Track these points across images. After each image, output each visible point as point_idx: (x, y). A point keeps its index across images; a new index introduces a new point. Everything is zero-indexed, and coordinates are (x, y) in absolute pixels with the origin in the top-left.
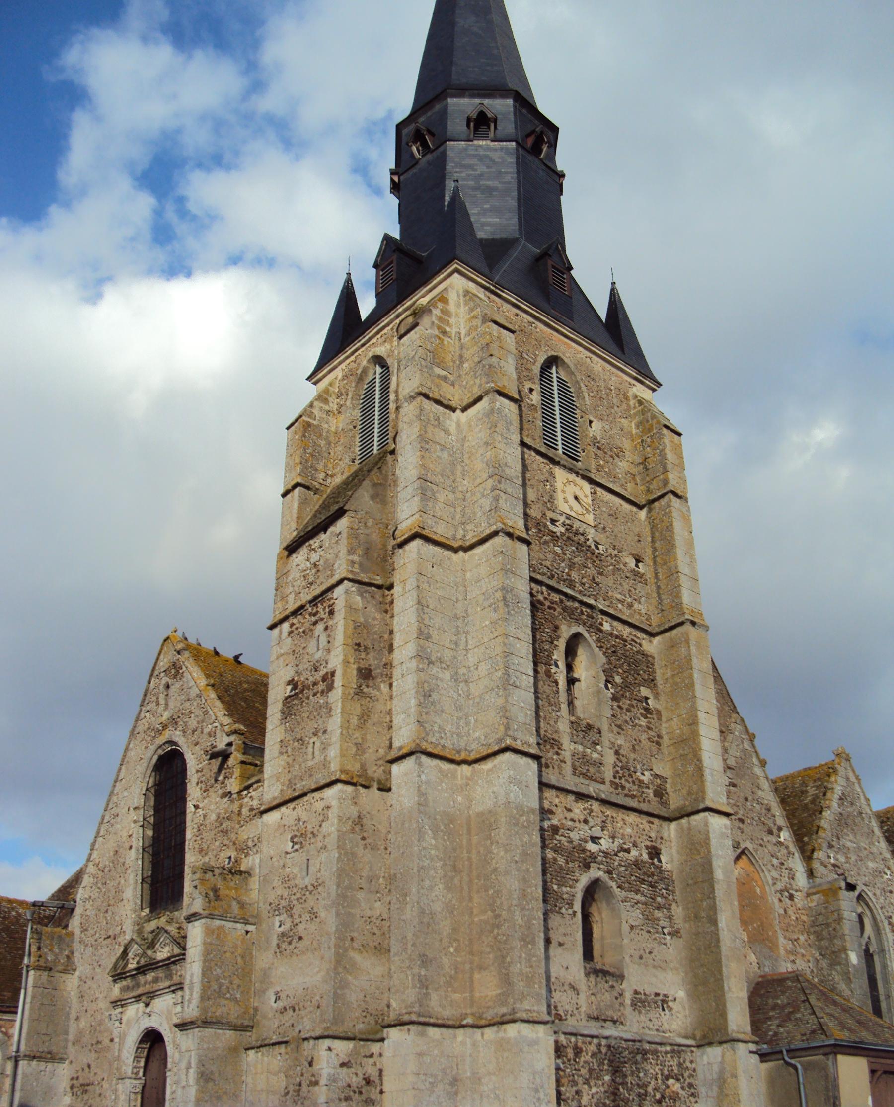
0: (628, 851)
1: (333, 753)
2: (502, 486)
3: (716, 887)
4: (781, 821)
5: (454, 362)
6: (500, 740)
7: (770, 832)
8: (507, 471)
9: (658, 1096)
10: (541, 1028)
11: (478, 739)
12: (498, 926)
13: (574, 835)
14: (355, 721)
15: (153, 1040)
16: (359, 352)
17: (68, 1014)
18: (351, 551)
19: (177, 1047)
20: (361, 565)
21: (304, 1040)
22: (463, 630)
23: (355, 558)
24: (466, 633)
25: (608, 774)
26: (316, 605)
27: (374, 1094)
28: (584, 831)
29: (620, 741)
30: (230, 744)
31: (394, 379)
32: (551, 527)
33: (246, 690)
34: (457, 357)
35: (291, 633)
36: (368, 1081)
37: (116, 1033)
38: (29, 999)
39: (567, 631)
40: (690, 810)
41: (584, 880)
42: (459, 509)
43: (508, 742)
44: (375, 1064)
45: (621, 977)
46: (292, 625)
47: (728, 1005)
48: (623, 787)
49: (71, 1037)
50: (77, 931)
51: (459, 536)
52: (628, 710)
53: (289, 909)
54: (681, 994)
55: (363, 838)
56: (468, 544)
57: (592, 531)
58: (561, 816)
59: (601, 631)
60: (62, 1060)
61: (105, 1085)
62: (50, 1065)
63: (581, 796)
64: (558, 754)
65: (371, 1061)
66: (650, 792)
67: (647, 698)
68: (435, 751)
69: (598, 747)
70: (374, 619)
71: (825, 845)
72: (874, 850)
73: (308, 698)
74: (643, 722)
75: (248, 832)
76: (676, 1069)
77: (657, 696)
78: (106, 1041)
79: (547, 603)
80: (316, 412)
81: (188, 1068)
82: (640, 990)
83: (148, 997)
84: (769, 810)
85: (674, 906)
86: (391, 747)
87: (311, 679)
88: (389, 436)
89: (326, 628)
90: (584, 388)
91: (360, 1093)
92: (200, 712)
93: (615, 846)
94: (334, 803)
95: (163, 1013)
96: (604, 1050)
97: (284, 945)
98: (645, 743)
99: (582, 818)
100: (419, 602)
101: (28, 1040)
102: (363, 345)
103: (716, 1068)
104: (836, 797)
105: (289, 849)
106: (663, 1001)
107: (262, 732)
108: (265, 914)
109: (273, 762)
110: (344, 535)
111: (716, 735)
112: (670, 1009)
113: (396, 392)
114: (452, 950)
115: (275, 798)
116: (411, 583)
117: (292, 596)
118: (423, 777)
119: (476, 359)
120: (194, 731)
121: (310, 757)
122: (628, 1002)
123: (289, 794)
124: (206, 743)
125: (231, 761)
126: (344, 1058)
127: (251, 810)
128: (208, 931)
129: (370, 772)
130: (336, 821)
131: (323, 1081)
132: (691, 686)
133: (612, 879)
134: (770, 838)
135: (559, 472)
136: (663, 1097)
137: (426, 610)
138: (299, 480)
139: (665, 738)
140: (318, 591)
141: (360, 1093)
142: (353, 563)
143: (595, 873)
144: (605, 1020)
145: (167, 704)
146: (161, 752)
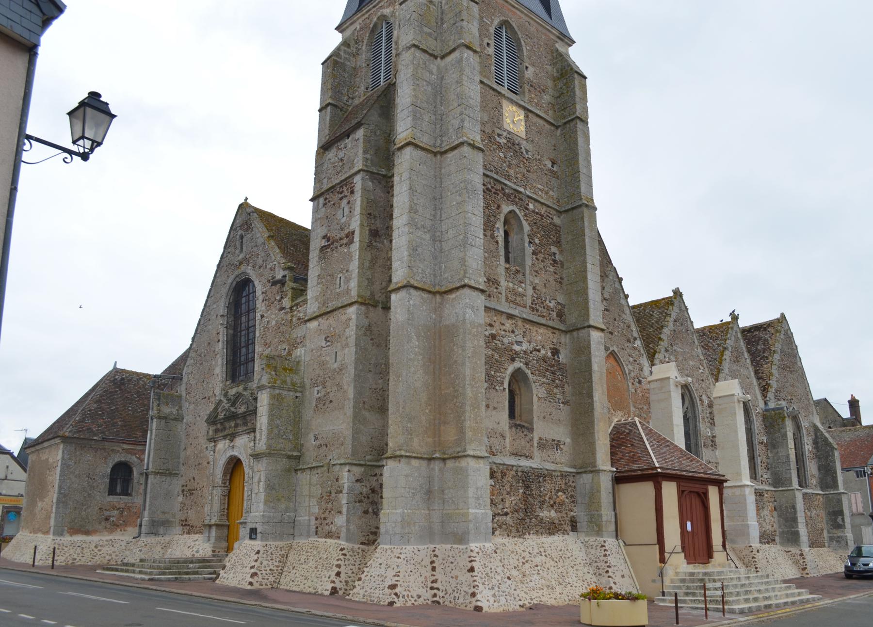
0: (539, 351)
1: (353, 284)
2: (467, 112)
3: (593, 375)
4: (635, 334)
5: (437, 23)
6: (461, 280)
7: (629, 341)
8: (471, 101)
9: (552, 502)
10: (481, 461)
11: (447, 278)
12: (456, 397)
13: (506, 341)
14: (367, 264)
15: (234, 465)
16: (371, 12)
17: (179, 445)
18: (365, 152)
19: (252, 468)
20: (372, 161)
21: (334, 465)
22: (443, 221)
23: (368, 156)
24: (441, 209)
25: (529, 302)
26: (342, 187)
27: (377, 498)
28: (512, 338)
29: (537, 281)
30: (285, 276)
31: (395, 33)
32: (498, 139)
33: (295, 240)
34: (439, 19)
35: (325, 204)
36: (373, 491)
37: (211, 459)
38: (153, 437)
39: (506, 208)
40: (579, 326)
41: (511, 369)
42: (438, 126)
43: (466, 281)
44: (377, 480)
45: (531, 430)
46: (326, 199)
47: (597, 449)
48: (537, 311)
49: (181, 461)
50: (184, 394)
51: (438, 145)
52: (543, 261)
53: (324, 384)
54: (568, 440)
55: (372, 339)
56: (443, 150)
57: (525, 142)
58: (498, 328)
59: (527, 209)
60: (176, 475)
61: (205, 490)
62: (168, 478)
63: (510, 316)
64: (497, 288)
65: (375, 478)
66: (554, 314)
67: (555, 254)
68: (419, 286)
69: (523, 285)
70: (380, 197)
71: (663, 350)
72: (694, 353)
73: (336, 248)
74: (552, 269)
75: (298, 332)
76: (563, 487)
77: (561, 252)
78: (205, 463)
79: (493, 190)
80: (342, 53)
81: (259, 482)
82: (543, 437)
83: (232, 437)
84: (629, 327)
85: (566, 386)
86: (390, 281)
87: (339, 235)
88: (392, 71)
89: (349, 203)
90: (523, 44)
91: (368, 498)
92: (263, 254)
93: (531, 348)
94: (354, 317)
95: (242, 446)
96: (520, 474)
97: (320, 406)
98: (553, 282)
99: (511, 329)
100: (410, 189)
101: (154, 462)
102: (374, 7)
103: (588, 486)
104: (672, 319)
105: (324, 345)
106: (557, 445)
107: (306, 268)
108: (308, 386)
109: (313, 290)
110: (361, 141)
111: (598, 279)
112: (562, 449)
113: (397, 43)
114: (427, 411)
115: (314, 312)
116: (405, 176)
117: (326, 180)
118: (411, 302)
119: (452, 22)
120: (260, 267)
121: (338, 286)
122: (535, 444)
123: (324, 310)
124: (268, 275)
125: (286, 288)
126: (358, 477)
127: (299, 319)
128: (273, 397)
129: (377, 298)
130: (354, 328)
131: (345, 491)
132: (583, 247)
133: (528, 368)
134: (628, 344)
135: (505, 103)
136: (555, 503)
137: (415, 194)
138: (330, 101)
139: (566, 279)
140: (343, 178)
141: (368, 498)
142: (367, 159)
143: (518, 364)
144: (521, 456)
145: (242, 248)
146: (238, 279)
